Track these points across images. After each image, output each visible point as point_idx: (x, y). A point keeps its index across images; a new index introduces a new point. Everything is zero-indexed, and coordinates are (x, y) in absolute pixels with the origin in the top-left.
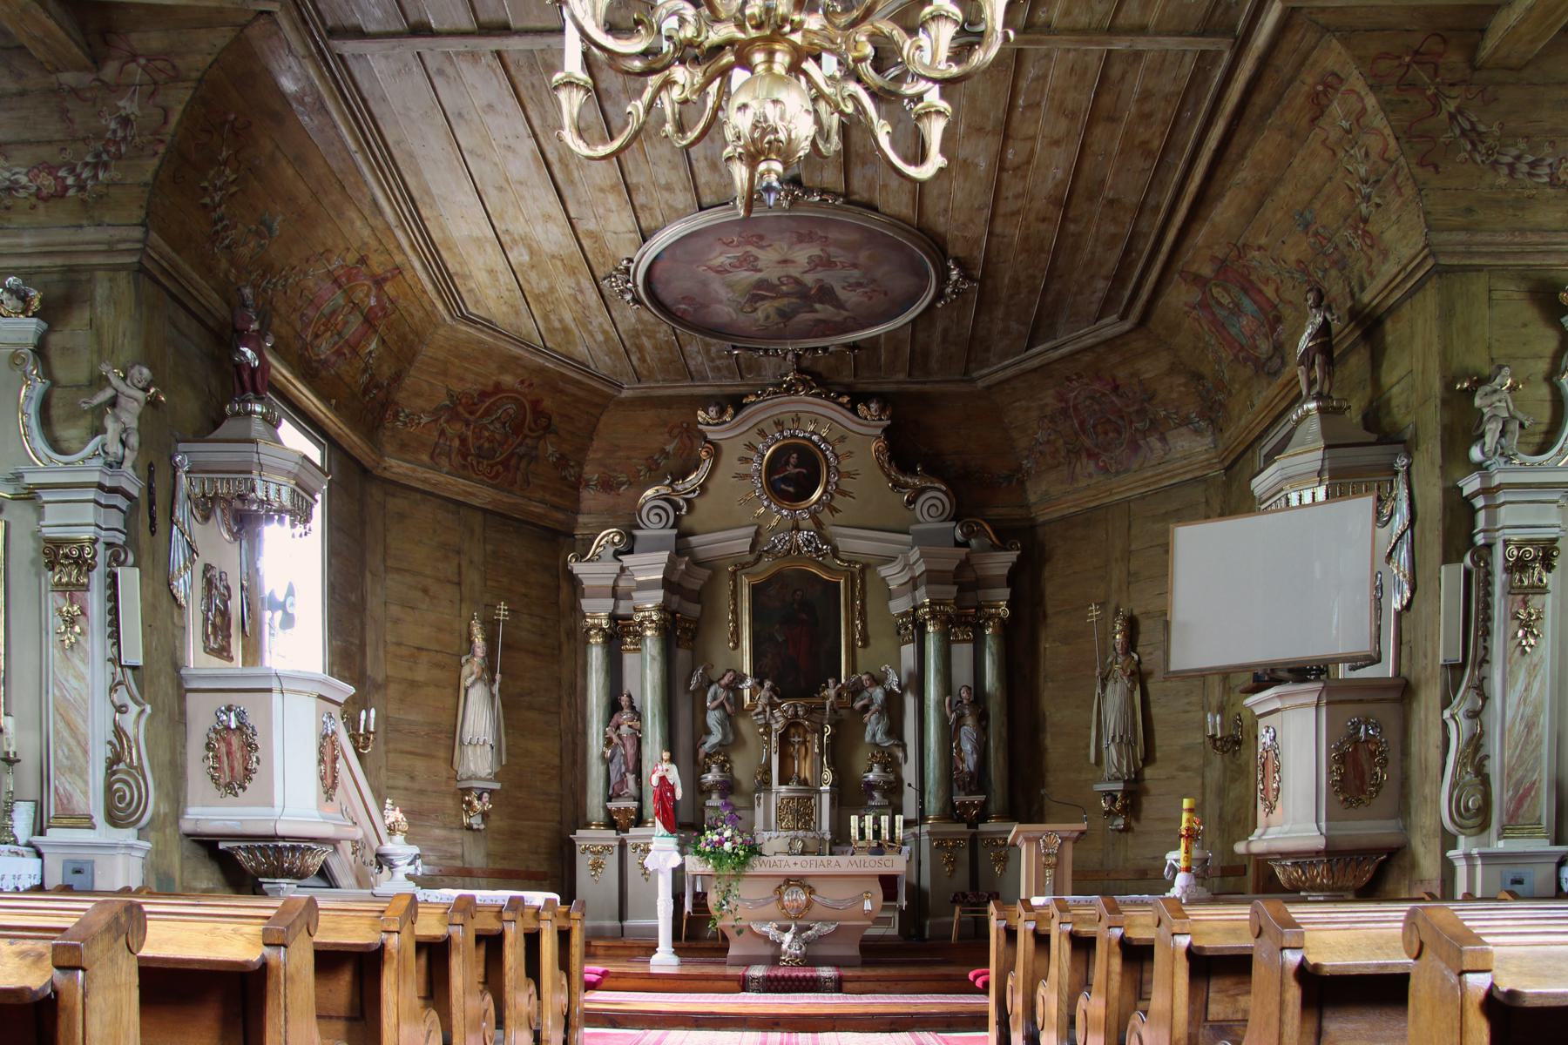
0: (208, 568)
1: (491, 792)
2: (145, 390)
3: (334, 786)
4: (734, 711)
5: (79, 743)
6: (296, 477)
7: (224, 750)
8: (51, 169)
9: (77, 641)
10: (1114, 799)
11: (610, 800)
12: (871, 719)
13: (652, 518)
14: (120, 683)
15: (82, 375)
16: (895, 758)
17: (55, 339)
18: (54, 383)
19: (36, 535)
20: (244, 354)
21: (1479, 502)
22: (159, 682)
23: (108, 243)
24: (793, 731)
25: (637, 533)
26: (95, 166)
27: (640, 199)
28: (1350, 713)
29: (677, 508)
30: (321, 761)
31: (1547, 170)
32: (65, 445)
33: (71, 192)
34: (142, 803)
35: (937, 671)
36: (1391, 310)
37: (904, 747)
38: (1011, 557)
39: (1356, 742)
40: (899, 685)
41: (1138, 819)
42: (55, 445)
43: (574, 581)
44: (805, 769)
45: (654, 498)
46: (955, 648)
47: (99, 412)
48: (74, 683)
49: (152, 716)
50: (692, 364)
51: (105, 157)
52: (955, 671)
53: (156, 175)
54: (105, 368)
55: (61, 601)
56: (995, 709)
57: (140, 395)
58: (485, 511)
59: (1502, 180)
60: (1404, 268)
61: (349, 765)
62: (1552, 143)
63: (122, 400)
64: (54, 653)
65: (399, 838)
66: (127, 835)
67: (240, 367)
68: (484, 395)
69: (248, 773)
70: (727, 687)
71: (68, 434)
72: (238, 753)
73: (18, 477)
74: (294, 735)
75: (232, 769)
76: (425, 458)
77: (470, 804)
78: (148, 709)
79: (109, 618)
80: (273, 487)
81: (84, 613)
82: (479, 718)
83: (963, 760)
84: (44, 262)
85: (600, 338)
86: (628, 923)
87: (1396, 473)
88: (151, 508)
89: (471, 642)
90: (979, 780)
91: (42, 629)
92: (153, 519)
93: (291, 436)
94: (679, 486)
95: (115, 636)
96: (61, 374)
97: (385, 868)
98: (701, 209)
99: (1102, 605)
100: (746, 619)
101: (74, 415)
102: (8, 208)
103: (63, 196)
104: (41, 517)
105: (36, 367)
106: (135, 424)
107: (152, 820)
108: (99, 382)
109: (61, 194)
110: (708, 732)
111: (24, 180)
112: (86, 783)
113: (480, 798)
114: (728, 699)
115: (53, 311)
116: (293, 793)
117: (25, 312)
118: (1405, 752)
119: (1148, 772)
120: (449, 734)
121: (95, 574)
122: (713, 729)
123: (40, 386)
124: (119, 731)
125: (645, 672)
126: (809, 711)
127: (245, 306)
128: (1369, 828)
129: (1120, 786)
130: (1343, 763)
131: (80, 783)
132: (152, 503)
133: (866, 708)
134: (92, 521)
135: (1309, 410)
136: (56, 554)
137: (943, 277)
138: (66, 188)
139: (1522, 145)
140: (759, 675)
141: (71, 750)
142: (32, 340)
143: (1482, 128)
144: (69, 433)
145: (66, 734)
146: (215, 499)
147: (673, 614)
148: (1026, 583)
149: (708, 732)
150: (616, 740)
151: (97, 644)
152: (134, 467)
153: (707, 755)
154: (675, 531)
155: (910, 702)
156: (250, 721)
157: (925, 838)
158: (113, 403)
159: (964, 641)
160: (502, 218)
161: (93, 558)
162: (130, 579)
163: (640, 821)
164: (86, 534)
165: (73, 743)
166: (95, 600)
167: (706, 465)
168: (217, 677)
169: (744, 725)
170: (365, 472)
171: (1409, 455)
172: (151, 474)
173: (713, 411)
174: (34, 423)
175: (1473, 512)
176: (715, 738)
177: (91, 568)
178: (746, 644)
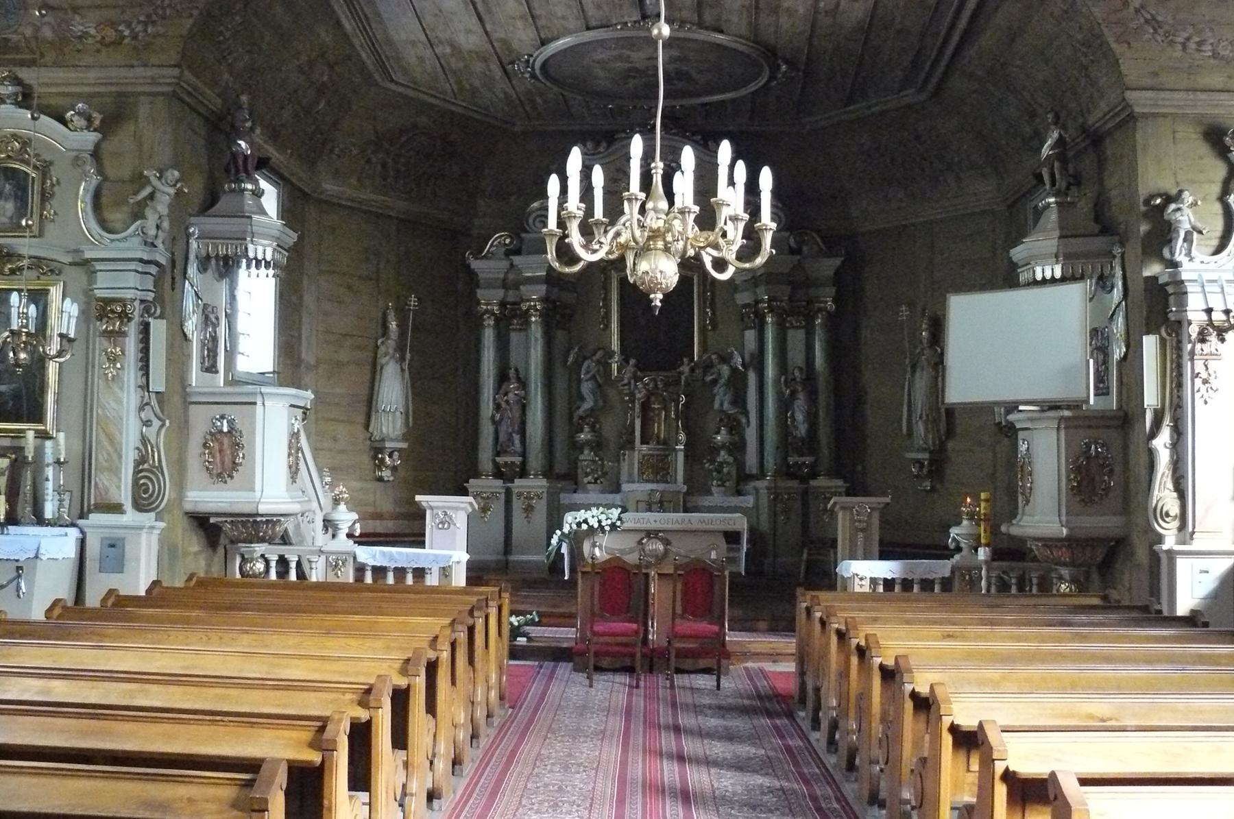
1: (399, 450)
4: (603, 382)
5: (116, 450)
7: (217, 448)
8: (113, 24)
10: (922, 466)
11: (498, 454)
12: (719, 390)
14: (147, 404)
15: (126, 173)
16: (739, 423)
18: (106, 179)
21: (1170, 289)
22: (172, 404)
23: (153, 78)
24: (653, 399)
25: (523, 235)
26: (146, 24)
27: (541, 22)
28: (1083, 437)
30: (290, 455)
31: (1210, 47)
32: (111, 225)
33: (126, 41)
35: (774, 355)
36: (1109, 133)
37: (746, 413)
38: (837, 262)
39: (1088, 458)
40: (743, 365)
41: (942, 482)
42: (103, 224)
43: (472, 278)
44: (660, 428)
46: (791, 333)
47: (142, 205)
48: (113, 405)
50: (573, 110)
51: (154, 17)
52: (790, 355)
53: (190, 30)
56: (822, 384)
58: (400, 220)
59: (1178, 53)
60: (1112, 109)
62: (1211, 29)
63: (158, 195)
64: (99, 383)
65: (342, 507)
66: (148, 518)
68: (402, 132)
69: (235, 465)
70: (598, 362)
72: (228, 454)
75: (223, 463)
76: (353, 181)
77: (382, 461)
79: (140, 355)
80: (260, 249)
81: (123, 353)
82: (393, 391)
83: (796, 428)
84: (102, 89)
85: (502, 96)
86: (513, 558)
87: (1114, 257)
88: (173, 271)
90: (810, 443)
92: (173, 278)
95: (145, 367)
96: (111, 172)
98: (588, 28)
99: (911, 305)
101: (119, 203)
102: (79, 51)
103: (120, 44)
109: (118, 43)
111: (92, 31)
112: (120, 479)
113: (390, 456)
114: (598, 371)
117: (88, 128)
118: (1126, 462)
119: (950, 445)
122: (586, 396)
123: (95, 180)
124: (144, 440)
125: (532, 352)
126: (667, 385)
127: (240, 107)
128: (1101, 523)
129: (926, 456)
130: (1080, 473)
131: (115, 480)
133: (715, 382)
135: (1049, 204)
136: (104, 309)
137: (775, 68)
138: (124, 38)
139: (1190, 30)
141: (109, 454)
142: (91, 147)
143: (1160, 18)
144: (116, 216)
147: (554, 302)
148: (848, 286)
149: (582, 398)
150: (504, 405)
151: (131, 376)
153: (581, 418)
155: (752, 377)
156: (238, 427)
157: (763, 492)
158: (151, 196)
159: (797, 328)
160: (433, 30)
162: (159, 329)
163: (523, 473)
164: (129, 294)
166: (131, 344)
169: (612, 393)
171: (1122, 245)
174: (89, 209)
175: (1167, 295)
176: (588, 405)
177: (130, 319)
178: (615, 326)
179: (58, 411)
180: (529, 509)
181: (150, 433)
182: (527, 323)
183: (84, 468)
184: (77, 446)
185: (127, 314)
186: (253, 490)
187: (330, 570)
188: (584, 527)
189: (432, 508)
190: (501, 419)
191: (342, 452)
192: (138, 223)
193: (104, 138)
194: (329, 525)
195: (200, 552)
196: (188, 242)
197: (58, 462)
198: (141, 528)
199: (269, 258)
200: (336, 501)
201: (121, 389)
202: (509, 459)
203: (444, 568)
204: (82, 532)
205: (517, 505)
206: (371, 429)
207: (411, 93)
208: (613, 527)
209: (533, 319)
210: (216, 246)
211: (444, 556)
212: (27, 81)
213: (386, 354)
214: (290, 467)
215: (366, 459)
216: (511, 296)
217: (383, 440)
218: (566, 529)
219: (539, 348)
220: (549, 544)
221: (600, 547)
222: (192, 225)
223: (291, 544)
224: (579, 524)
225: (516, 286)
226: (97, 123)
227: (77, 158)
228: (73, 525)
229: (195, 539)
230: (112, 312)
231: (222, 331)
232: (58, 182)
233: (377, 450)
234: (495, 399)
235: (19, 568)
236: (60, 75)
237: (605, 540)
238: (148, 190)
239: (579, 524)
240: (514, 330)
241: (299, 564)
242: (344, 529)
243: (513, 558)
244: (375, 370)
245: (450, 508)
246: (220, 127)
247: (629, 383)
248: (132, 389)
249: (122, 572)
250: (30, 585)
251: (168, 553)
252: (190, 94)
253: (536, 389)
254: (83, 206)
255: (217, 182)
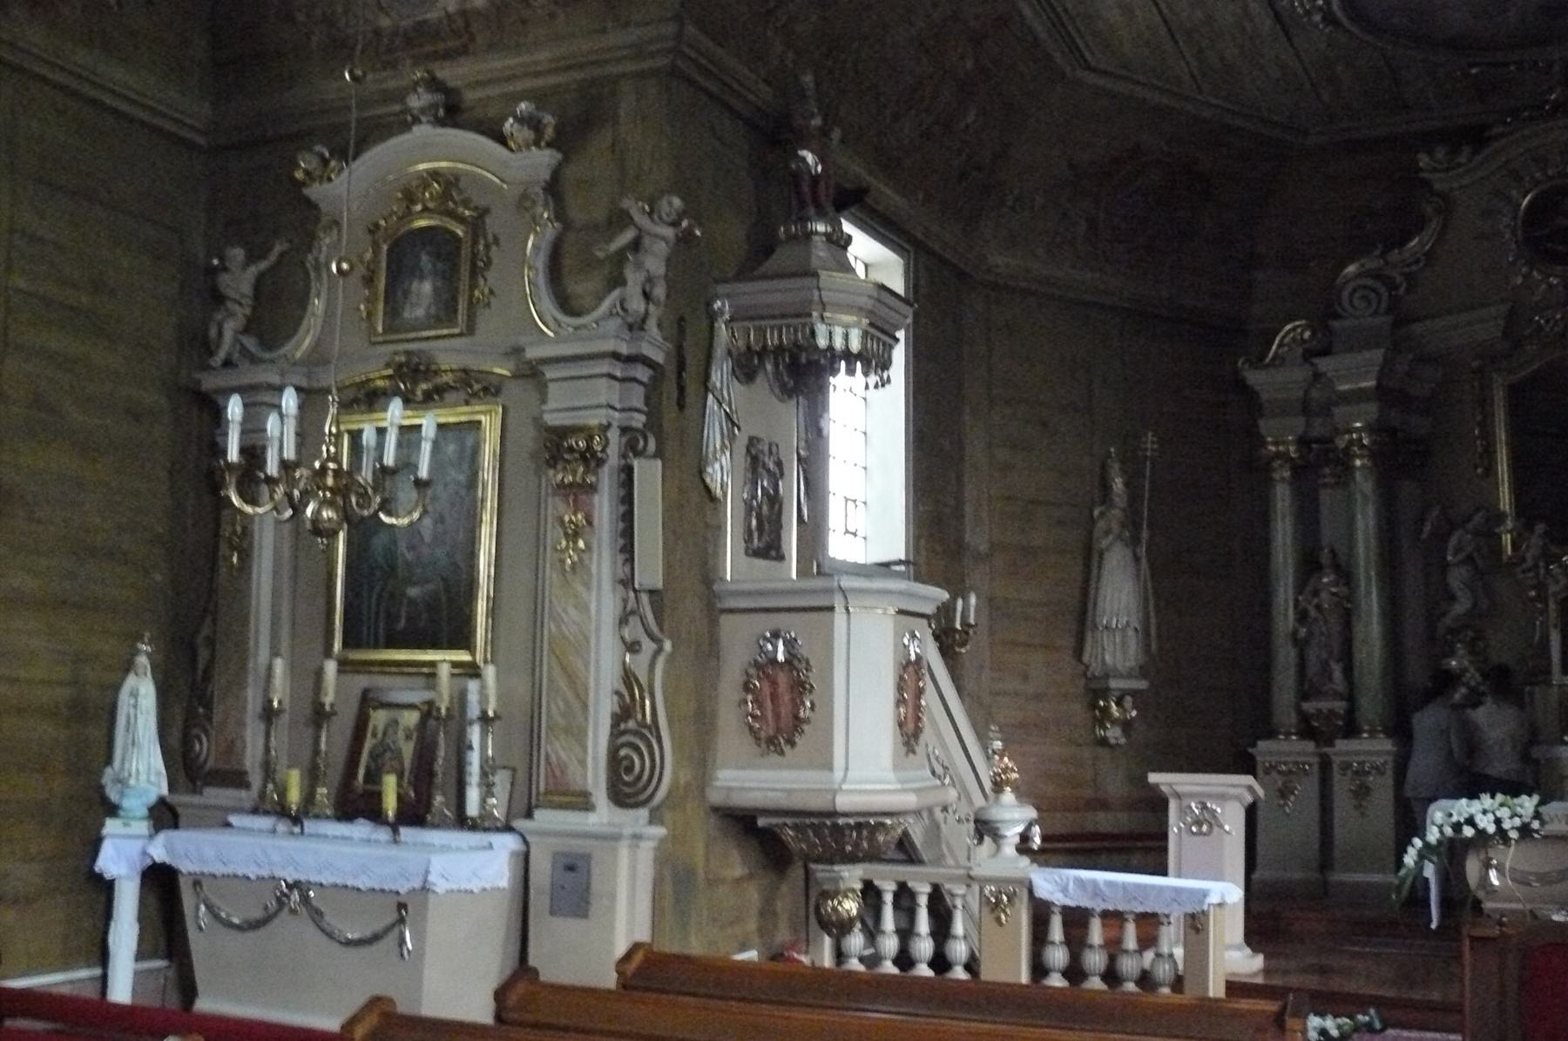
0: (753, 441)
1: (1134, 693)
2: (675, 224)
3: (917, 732)
4: (1486, 562)
5: (578, 696)
6: (870, 313)
7: (767, 691)
9: (581, 559)
11: (1304, 696)
13: (1356, 302)
14: (632, 612)
15: (600, 215)
17: (571, 172)
19: (538, 422)
20: (804, 159)
22: (683, 608)
25: (1336, 324)
29: (1392, 286)
30: (900, 701)
34: (656, 771)
42: (566, 304)
43: (1248, 395)
45: (1359, 275)
47: (620, 259)
49: (671, 658)
54: (626, 203)
55: (562, 507)
57: (669, 232)
61: (942, 696)
63: (647, 241)
64: (551, 575)
67: (797, 176)
69: (798, 723)
71: (580, 288)
72: (787, 704)
73: (517, 351)
74: (866, 659)
77: (1105, 711)
78: (668, 645)
79: (621, 542)
80: (838, 332)
81: (590, 523)
82: (1120, 595)
86: (1338, 876)
88: (680, 376)
89: (1106, 487)
91: (539, 542)
92: (681, 389)
93: (867, 252)
94: (1394, 256)
95: (628, 550)
96: (577, 215)
97: (987, 839)
100: (1502, 435)
101: (588, 264)
104: (544, 401)
105: (546, 206)
106: (662, 271)
107: (670, 793)
108: (620, 219)
110: (1452, 598)
112: (584, 748)
113: (1118, 704)
115: (568, 139)
116: (864, 758)
117: (537, 144)
120: (1081, 618)
121: (605, 471)
123: (550, 231)
124: (628, 677)
125: (1361, 524)
127: (802, 95)
131: (577, 749)
132: (681, 366)
134: (603, 400)
136: (559, 446)
140: (1526, 513)
141: (567, 703)
142: (545, 175)
145: (562, 683)
146: (763, 353)
149: (1452, 598)
150: (1313, 613)
151: (604, 564)
152: (659, 325)
154: (1389, 319)
156: (804, 650)
161: (603, 451)
162: (649, 475)
163: (1351, 729)
164: (593, 419)
165: (570, 695)
166: (604, 506)
167: (1434, 225)
168: (761, 593)
170: (962, 275)
172: (681, 331)
173: (1440, 153)
174: (541, 280)
176: (1461, 607)
177: (601, 462)
179: (494, 628)
180: (1362, 792)
181: (639, 663)
182: (1349, 469)
183: (528, 729)
184: (521, 686)
185: (594, 454)
186: (829, 767)
187: (986, 910)
188: (1468, 832)
189: (1178, 796)
190: (1310, 634)
191: (1038, 697)
192: (616, 293)
193: (566, 159)
194: (985, 829)
195: (751, 876)
196: (712, 328)
197: (484, 719)
198: (616, 838)
199: (855, 346)
200: (998, 787)
201: (587, 586)
202: (1324, 705)
203: (1193, 916)
204: (526, 842)
205: (1342, 786)
206: (1086, 658)
207: (1122, 87)
208: (1525, 830)
209: (1358, 463)
210: (761, 332)
211: (1192, 892)
212: (451, 84)
213: (1107, 532)
214: (901, 725)
215: (1078, 709)
216: (1318, 430)
217: (1107, 676)
218: (1433, 836)
219: (1371, 510)
220: (1399, 863)
221: (1500, 870)
222: (717, 297)
223: (920, 862)
224: (1457, 827)
225: (1326, 410)
226: (549, 133)
227: (524, 196)
228: (508, 828)
229: (735, 855)
230: (571, 450)
231: (792, 488)
232: (496, 241)
233: (1096, 692)
234: (1297, 602)
235: (402, 906)
236: (497, 63)
237: (1508, 856)
238: (628, 236)
239: (1457, 827)
240: (1325, 485)
241: (936, 897)
242: (1012, 833)
243: (1338, 876)
244: (1090, 558)
245: (1210, 796)
246: (775, 135)
247: (1536, 566)
248: (607, 584)
249: (585, 916)
250: (419, 937)
251: (676, 885)
252: (708, 73)
253: (1368, 585)
254: (534, 276)
255: (768, 223)
